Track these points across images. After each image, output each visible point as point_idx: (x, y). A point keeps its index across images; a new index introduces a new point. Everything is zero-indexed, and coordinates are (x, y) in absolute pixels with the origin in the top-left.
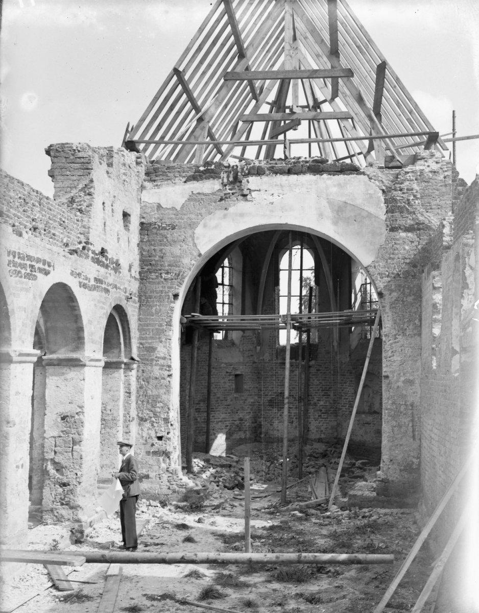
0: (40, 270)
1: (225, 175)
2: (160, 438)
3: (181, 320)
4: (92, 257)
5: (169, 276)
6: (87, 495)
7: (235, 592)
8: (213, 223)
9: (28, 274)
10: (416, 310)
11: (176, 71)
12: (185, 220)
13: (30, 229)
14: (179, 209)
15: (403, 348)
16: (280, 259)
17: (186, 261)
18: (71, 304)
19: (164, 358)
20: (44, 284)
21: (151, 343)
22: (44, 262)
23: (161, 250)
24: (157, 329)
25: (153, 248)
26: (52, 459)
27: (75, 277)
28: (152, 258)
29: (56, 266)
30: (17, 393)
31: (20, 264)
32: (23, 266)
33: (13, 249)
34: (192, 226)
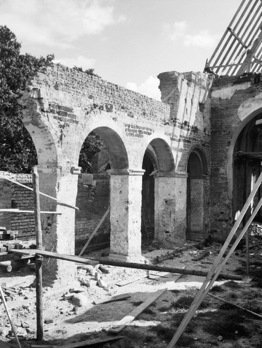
0: (145, 133)
1: (253, 79)
3: (233, 155)
4: (179, 126)
5: (225, 133)
7: (231, 290)
8: (247, 105)
9: (138, 135)
11: (229, 29)
12: (233, 104)
13: (141, 114)
17: (234, 125)
18: (167, 148)
19: (223, 174)
20: (148, 139)
21: (218, 166)
22: (148, 129)
23: (221, 121)
24: (219, 160)
25: (217, 119)
27: (168, 136)
28: (217, 125)
29: (155, 131)
30: (133, 189)
31: (133, 131)
32: (136, 131)
33: (128, 123)
34: (237, 107)
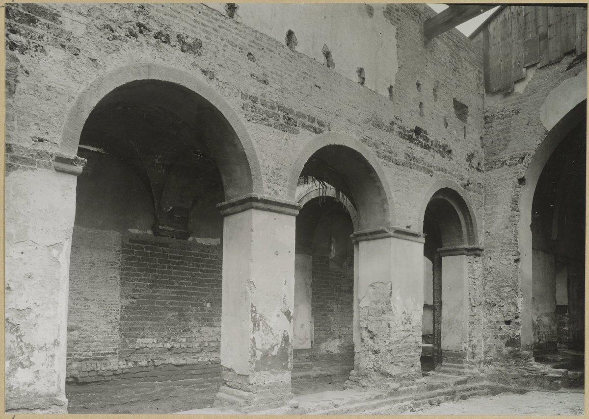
2: (508, 323)
6: (401, 364)
26: (366, 328)
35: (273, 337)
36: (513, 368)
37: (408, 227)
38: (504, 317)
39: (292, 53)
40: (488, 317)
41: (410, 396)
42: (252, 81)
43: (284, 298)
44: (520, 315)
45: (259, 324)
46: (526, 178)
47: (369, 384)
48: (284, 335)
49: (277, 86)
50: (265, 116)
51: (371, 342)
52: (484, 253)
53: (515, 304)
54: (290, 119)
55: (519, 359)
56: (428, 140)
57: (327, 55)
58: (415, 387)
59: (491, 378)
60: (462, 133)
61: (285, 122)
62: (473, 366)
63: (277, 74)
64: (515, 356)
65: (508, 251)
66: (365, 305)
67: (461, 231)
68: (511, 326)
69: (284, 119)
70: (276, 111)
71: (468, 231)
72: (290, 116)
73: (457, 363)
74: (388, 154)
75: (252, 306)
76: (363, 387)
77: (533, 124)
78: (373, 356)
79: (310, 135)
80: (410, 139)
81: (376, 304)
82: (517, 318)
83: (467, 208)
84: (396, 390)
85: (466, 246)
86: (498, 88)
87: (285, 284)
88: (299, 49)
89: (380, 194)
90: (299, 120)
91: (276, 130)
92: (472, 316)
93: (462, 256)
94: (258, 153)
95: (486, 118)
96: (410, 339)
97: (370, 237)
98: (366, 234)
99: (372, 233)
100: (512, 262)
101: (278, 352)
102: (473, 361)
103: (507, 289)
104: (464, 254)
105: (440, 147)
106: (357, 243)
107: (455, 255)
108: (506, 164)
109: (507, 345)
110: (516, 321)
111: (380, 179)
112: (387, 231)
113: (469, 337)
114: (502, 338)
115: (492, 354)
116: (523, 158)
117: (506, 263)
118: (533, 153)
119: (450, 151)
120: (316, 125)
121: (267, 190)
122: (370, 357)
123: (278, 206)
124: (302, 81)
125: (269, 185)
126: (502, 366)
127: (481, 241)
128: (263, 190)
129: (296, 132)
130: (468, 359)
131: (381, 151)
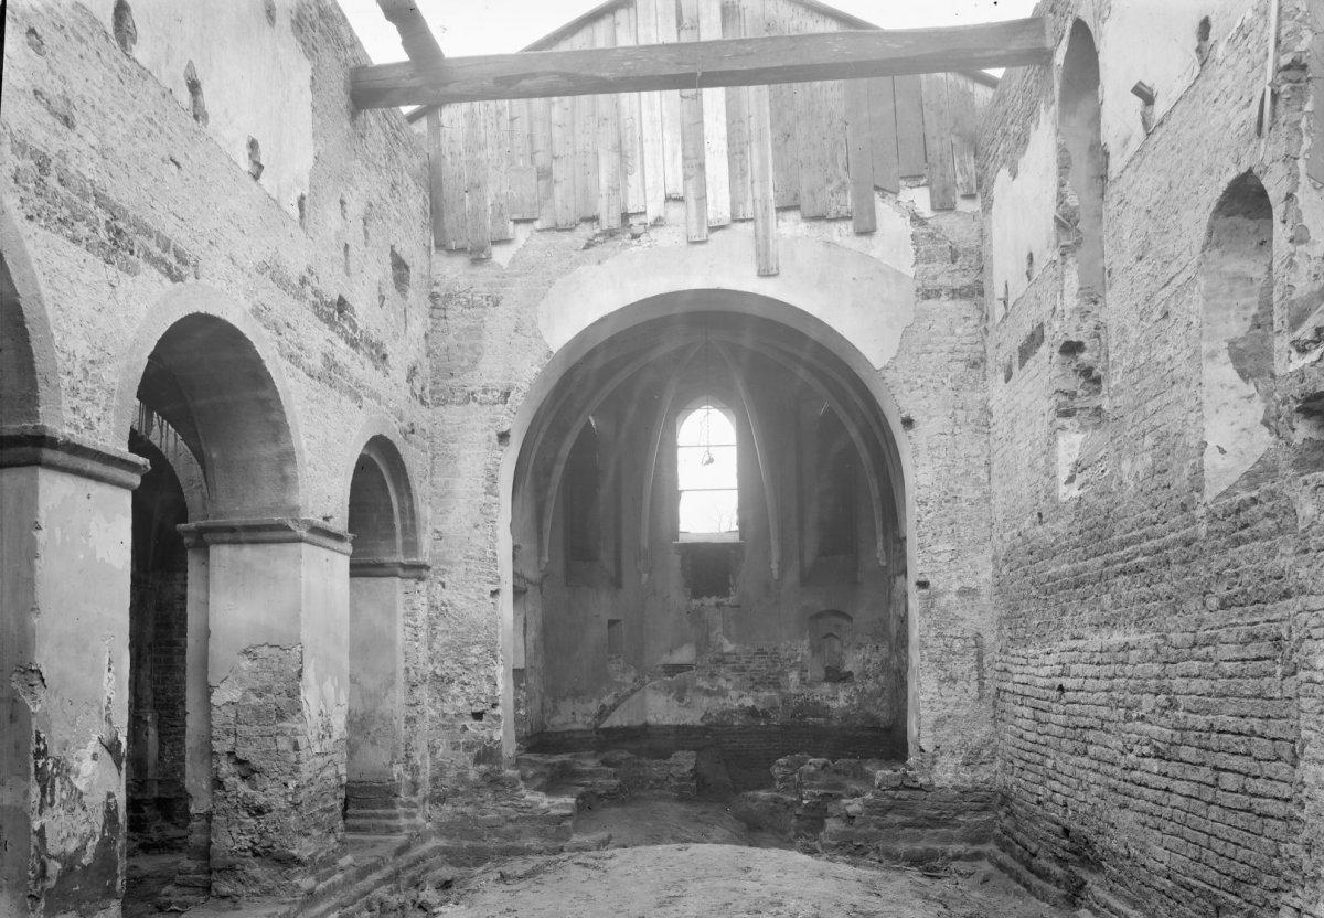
2: (478, 716)
6: (315, 832)
10: (979, 452)
14: (505, 266)
15: (954, 526)
16: (678, 427)
23: (472, 348)
26: (231, 754)
35: (83, 817)
36: (489, 805)
37: (326, 519)
38: (471, 705)
39: (125, 61)
40: (438, 705)
41: (334, 900)
42: (38, 109)
43: (107, 708)
44: (500, 701)
45: (53, 786)
46: (511, 434)
47: (241, 889)
48: (109, 805)
49: (93, 140)
50: (66, 212)
51: (243, 788)
52: (431, 574)
53: (491, 679)
54: (119, 232)
55: (500, 788)
56: (354, 328)
57: (194, 87)
58: (339, 877)
59: (445, 830)
60: (401, 320)
61: (110, 240)
62: (414, 810)
63: (93, 106)
64: (494, 782)
65: (480, 573)
66: (229, 699)
67: (393, 527)
68: (484, 722)
69: (108, 231)
70: (91, 206)
71: (404, 527)
72: (121, 225)
73: (382, 807)
74: (297, 351)
75: (38, 740)
76: (224, 897)
77: (525, 332)
78: (252, 820)
79: (160, 281)
80: (329, 320)
81: (260, 695)
82: (494, 706)
83: (407, 480)
84: (310, 893)
85: (400, 558)
86: (461, 244)
87: (110, 669)
88: (141, 52)
89: (276, 440)
90: (139, 240)
91: (90, 256)
92: (412, 705)
93: (298, 545)
94: (51, 313)
95: (433, 297)
96: (329, 772)
97: (243, 536)
98: (232, 529)
99: (249, 528)
100: (487, 596)
101: (95, 855)
102: (414, 799)
103: (476, 650)
104: (396, 575)
105: (372, 347)
106: (203, 548)
107: (378, 576)
108: (475, 399)
109: (478, 760)
110: (494, 712)
111: (282, 407)
112: (292, 526)
113: (406, 750)
114: (469, 747)
115: (447, 782)
116: (507, 394)
117: (475, 597)
118: (526, 387)
119: (385, 357)
120: (172, 260)
121: (69, 416)
122: (241, 824)
123: (99, 461)
124: (144, 138)
125: (76, 402)
126: (467, 804)
127: (427, 549)
128: (59, 418)
129: (131, 270)
130: (403, 797)
131: (285, 342)
